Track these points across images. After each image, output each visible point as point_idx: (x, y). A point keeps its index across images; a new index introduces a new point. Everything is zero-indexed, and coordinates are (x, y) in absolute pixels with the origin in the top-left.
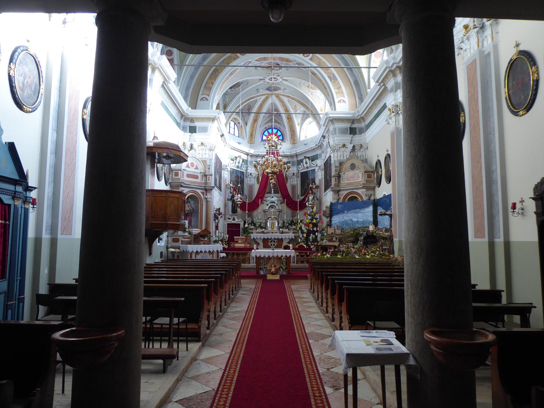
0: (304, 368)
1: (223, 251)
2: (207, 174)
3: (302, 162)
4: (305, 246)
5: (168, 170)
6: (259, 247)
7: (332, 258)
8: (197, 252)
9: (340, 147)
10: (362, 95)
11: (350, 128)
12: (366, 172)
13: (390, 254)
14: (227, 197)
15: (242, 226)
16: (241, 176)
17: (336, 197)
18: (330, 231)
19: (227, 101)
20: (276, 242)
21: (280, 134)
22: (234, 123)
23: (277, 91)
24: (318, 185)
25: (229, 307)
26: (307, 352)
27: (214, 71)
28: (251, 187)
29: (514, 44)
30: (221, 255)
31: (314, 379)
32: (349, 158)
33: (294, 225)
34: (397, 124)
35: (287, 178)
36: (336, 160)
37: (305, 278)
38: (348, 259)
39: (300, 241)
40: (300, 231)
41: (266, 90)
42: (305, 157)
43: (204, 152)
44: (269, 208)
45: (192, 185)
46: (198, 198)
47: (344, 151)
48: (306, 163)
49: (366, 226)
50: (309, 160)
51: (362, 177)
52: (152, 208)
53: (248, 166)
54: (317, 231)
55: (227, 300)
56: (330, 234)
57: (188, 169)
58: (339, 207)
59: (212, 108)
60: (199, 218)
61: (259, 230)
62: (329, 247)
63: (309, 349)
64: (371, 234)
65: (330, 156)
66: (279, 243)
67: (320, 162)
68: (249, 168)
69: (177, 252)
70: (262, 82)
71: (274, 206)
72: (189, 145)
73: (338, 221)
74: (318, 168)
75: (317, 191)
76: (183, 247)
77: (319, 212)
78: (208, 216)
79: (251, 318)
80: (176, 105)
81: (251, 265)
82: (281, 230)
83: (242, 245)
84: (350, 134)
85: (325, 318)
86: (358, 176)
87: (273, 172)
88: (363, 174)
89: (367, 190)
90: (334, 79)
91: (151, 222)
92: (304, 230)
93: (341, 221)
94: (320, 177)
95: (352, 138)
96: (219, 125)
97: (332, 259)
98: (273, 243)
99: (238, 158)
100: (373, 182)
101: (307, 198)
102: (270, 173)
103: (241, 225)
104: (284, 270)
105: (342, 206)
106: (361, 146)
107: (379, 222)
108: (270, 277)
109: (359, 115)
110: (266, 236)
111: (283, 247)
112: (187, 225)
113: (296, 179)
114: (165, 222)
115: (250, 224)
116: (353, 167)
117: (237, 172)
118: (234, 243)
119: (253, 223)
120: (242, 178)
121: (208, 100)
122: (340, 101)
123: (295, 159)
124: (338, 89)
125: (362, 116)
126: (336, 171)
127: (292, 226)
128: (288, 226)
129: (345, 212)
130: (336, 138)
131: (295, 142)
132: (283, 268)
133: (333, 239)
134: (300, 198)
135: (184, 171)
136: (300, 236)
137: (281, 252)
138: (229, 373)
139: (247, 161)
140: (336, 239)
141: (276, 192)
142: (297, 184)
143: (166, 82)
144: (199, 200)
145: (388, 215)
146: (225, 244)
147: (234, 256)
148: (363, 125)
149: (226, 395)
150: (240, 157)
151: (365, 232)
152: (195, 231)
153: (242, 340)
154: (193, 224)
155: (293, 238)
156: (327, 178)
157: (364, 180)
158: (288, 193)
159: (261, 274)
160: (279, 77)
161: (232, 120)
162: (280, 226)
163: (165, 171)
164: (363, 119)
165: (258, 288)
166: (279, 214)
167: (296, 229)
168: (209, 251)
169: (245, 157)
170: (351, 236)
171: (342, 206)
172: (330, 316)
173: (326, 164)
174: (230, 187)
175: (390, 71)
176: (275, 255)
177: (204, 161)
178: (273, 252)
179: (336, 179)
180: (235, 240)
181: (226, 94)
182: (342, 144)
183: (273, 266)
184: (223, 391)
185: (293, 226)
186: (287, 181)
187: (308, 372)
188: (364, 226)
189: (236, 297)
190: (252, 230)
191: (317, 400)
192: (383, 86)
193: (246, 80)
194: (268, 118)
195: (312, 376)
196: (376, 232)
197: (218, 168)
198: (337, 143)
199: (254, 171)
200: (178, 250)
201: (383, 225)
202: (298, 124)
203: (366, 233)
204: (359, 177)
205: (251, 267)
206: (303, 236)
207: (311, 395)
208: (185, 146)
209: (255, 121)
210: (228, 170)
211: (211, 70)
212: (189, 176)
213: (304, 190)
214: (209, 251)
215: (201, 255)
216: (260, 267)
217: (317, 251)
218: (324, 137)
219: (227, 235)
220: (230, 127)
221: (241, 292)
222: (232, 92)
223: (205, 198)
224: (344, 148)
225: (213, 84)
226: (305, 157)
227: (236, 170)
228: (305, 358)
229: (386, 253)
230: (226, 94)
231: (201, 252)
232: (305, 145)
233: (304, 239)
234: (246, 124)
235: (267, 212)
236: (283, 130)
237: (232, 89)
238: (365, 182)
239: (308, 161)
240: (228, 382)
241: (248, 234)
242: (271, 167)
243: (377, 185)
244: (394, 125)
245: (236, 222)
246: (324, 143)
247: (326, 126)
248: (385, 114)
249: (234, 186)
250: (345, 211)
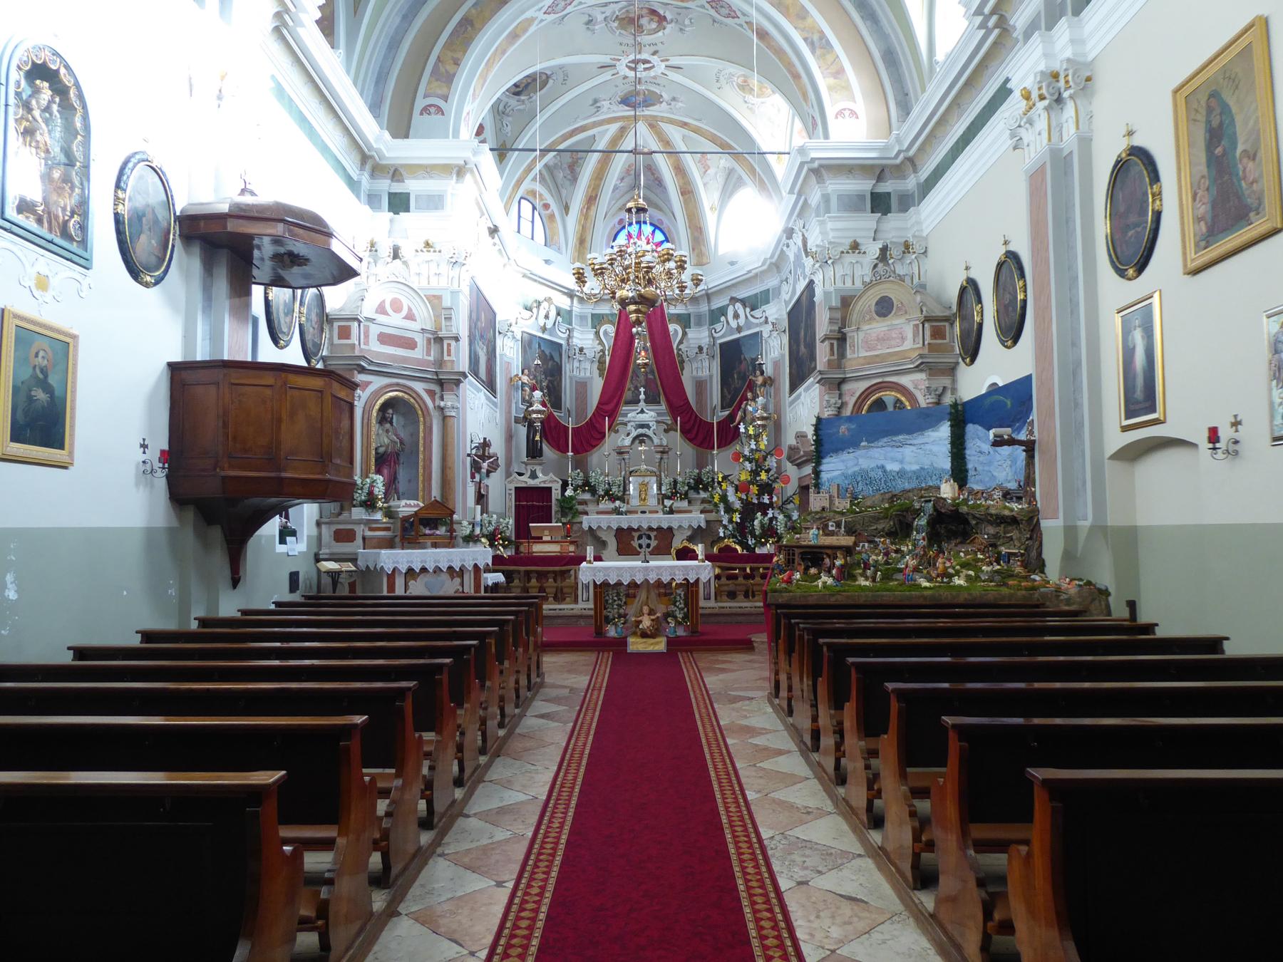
2: (442, 334)
3: (725, 314)
5: (314, 317)
6: (605, 554)
7: (842, 589)
8: (410, 571)
9: (842, 252)
11: (872, 193)
12: (928, 319)
13: (1029, 572)
14: (514, 414)
15: (556, 494)
16: (553, 354)
17: (834, 400)
19: (509, 135)
20: (653, 538)
22: (531, 206)
23: (651, 108)
25: (481, 785)
26: (740, 823)
27: (460, 24)
28: (582, 387)
29: (1124, 131)
30: (487, 578)
32: (872, 281)
33: (705, 489)
35: (682, 362)
36: (832, 289)
37: (746, 646)
38: (894, 591)
40: (722, 506)
44: (633, 442)
45: (395, 368)
46: (414, 408)
47: (854, 261)
48: (736, 316)
49: (930, 487)
50: (745, 306)
51: (915, 335)
52: (225, 425)
53: (573, 329)
54: (771, 505)
56: (817, 513)
57: (381, 318)
58: (843, 429)
59: (456, 134)
61: (606, 505)
62: (829, 551)
63: (747, 817)
65: (810, 285)
66: (662, 541)
67: (777, 311)
68: (576, 334)
70: (607, 76)
72: (389, 250)
73: (839, 472)
74: (770, 327)
75: (767, 393)
76: (367, 556)
77: (775, 449)
78: (449, 464)
79: (581, 758)
80: (339, 117)
81: (581, 605)
82: (668, 503)
83: (553, 549)
84: (872, 212)
85: (836, 805)
86: (901, 333)
87: (641, 296)
88: (917, 326)
89: (930, 375)
90: (821, 48)
91: (223, 473)
92: (733, 502)
93: (850, 472)
95: (878, 222)
97: (844, 591)
98: (644, 541)
99: (545, 305)
102: (633, 301)
103: (553, 491)
104: (680, 623)
105: (853, 427)
106: (907, 247)
107: (971, 473)
108: (636, 645)
110: (624, 522)
111: (673, 551)
112: (379, 490)
113: (706, 364)
114: (273, 474)
115: (581, 487)
116: (885, 307)
117: (542, 344)
118: (529, 543)
119: (587, 486)
122: (840, 113)
123: (704, 308)
124: (835, 78)
125: (911, 153)
126: (832, 321)
127: (699, 493)
128: (686, 494)
129: (863, 444)
130: (830, 225)
131: (705, 261)
132: (675, 617)
134: (720, 414)
139: (570, 312)
140: (838, 525)
142: (711, 377)
145: (1020, 443)
146: (501, 545)
147: (529, 581)
148: (911, 183)
149: (544, 873)
150: (549, 300)
151: (931, 504)
152: (407, 505)
154: (402, 485)
155: (703, 525)
156: (798, 352)
157: (921, 345)
158: (687, 399)
159: (608, 635)
160: (655, 57)
161: (526, 197)
162: (663, 492)
163: (303, 319)
164: (912, 163)
165: (598, 685)
166: (661, 458)
167: (710, 502)
168: (450, 568)
169: (564, 302)
170: (885, 515)
171: (853, 427)
172: (829, 763)
173: (794, 314)
174: (523, 383)
176: (652, 578)
177: (434, 296)
178: (646, 569)
179: (832, 345)
181: (503, 113)
182: (848, 242)
183: (646, 609)
185: (701, 491)
186: (683, 369)
187: (749, 888)
188: (923, 485)
189: (518, 731)
190: (586, 504)
191: (751, 880)
192: (996, 26)
193: (561, 67)
194: (626, 193)
196: (969, 501)
197: (482, 324)
198: (832, 240)
199: (591, 342)
200: (349, 567)
201: (987, 479)
204: (903, 339)
205: (579, 613)
206: (731, 521)
208: (376, 251)
209: (591, 200)
210: (514, 338)
212: (384, 339)
213: (729, 393)
214: (450, 568)
215: (422, 579)
218: (789, 233)
220: (519, 217)
221: (539, 706)
222: (521, 107)
223: (439, 407)
224: (854, 252)
225: (457, 63)
227: (540, 337)
231: (424, 570)
232: (732, 263)
234: (566, 208)
235: (628, 452)
236: (671, 227)
237: (522, 98)
238: (926, 351)
239: (741, 311)
240: (524, 924)
241: (573, 517)
242: (634, 281)
243: (963, 359)
244: (1045, 141)
246: (788, 253)
247: (800, 194)
248: (1006, 115)
250: (862, 441)
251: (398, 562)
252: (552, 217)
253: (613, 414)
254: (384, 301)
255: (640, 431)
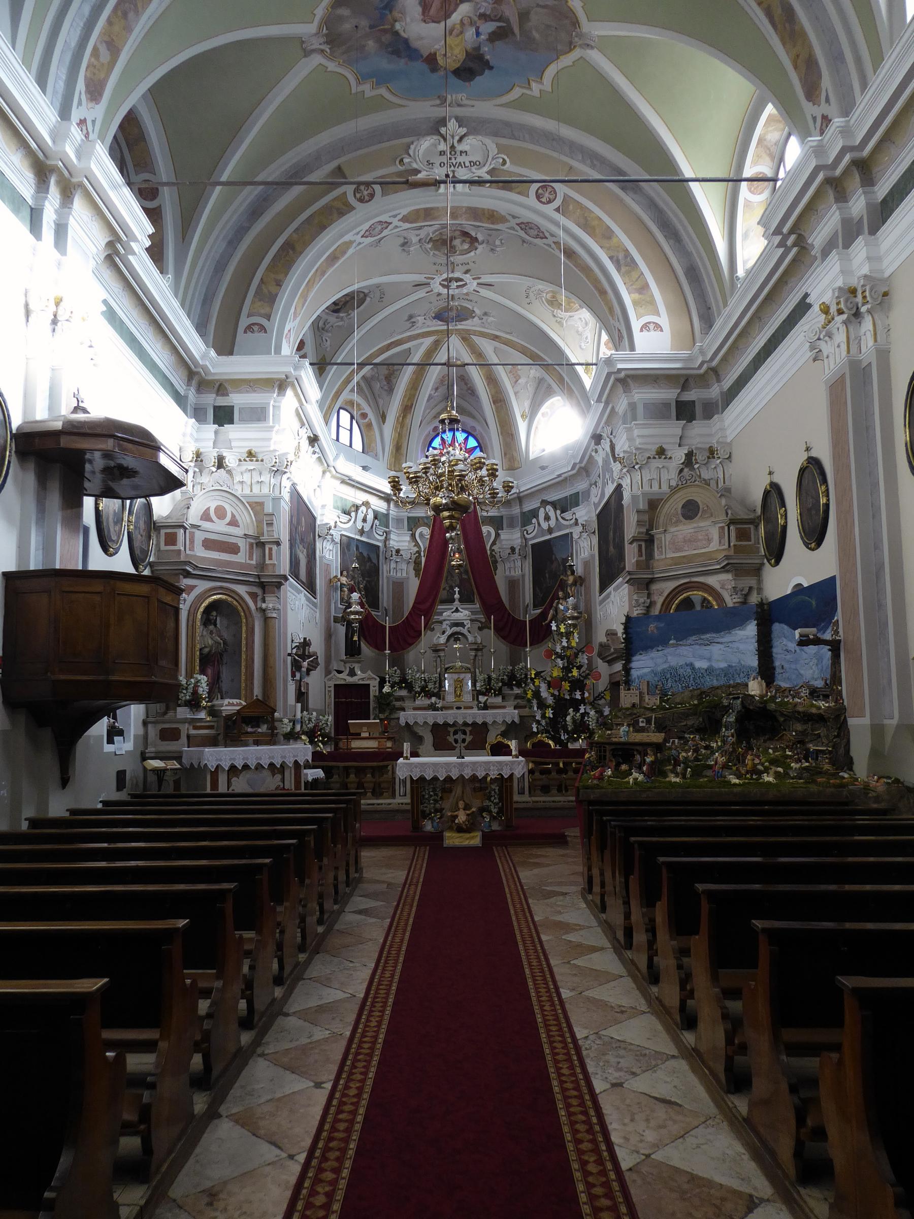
0: (536, 1011)
1: (317, 763)
2: (263, 539)
4: (551, 742)
5: (142, 525)
8: (233, 768)
9: (649, 458)
10: (710, 308)
11: (676, 401)
12: (732, 522)
13: (837, 769)
14: (333, 614)
15: (374, 691)
18: (627, 699)
21: (476, 444)
24: (580, 574)
27: (282, 248)
28: (399, 587)
30: (307, 774)
31: (559, 1036)
32: (678, 485)
33: (519, 685)
34: (854, 350)
35: (495, 562)
36: (640, 493)
37: (560, 840)
39: (535, 730)
41: (434, 318)
42: (544, 503)
43: (256, 478)
46: (240, 616)
47: (661, 466)
48: (547, 518)
49: (738, 684)
50: (555, 509)
51: (721, 537)
54: (583, 701)
55: (342, 887)
56: (627, 709)
57: (206, 525)
58: (652, 627)
60: (243, 667)
61: (422, 701)
64: (761, 706)
67: (586, 513)
68: (392, 536)
69: (171, 769)
70: (421, 293)
71: (462, 634)
73: (649, 670)
74: (580, 528)
81: (398, 800)
82: (482, 699)
83: (372, 744)
84: (677, 420)
86: (707, 535)
87: (454, 502)
89: (736, 575)
93: (659, 669)
94: (586, 554)
95: (683, 429)
96: (301, 405)
97: (655, 788)
98: (460, 736)
99: (363, 509)
100: (754, 550)
101: (551, 612)
102: (446, 507)
103: (372, 688)
105: (662, 625)
107: (778, 670)
108: (452, 839)
109: (706, 362)
110: (440, 717)
111: (488, 746)
112: (203, 689)
114: (101, 678)
116: (691, 510)
118: (347, 739)
119: (404, 682)
120: (375, 561)
121: (265, 330)
123: (516, 510)
124: (640, 293)
125: (714, 363)
127: (512, 689)
128: (500, 689)
129: (671, 642)
130: (636, 432)
131: (516, 465)
133: (638, 722)
135: (194, 530)
136: (535, 717)
137: (485, 763)
138: (366, 1026)
139: (387, 515)
140: (648, 721)
141: (466, 599)
142: (523, 576)
143: (119, 246)
144: (242, 614)
145: (826, 642)
148: (714, 392)
149: (361, 1073)
150: (366, 504)
151: (739, 701)
152: (230, 704)
153: (382, 996)
154: (225, 685)
155: (517, 720)
157: (726, 546)
159: (424, 830)
160: (468, 275)
162: (478, 689)
163: (132, 527)
164: (715, 373)
166: (476, 656)
168: (272, 765)
169: (379, 505)
170: (694, 711)
171: (662, 625)
173: (602, 516)
175: (828, 183)
176: (467, 774)
177: (256, 503)
179: (640, 546)
180: (352, 731)
182: (655, 448)
183: (461, 804)
184: (354, 1066)
185: (515, 688)
186: (496, 569)
187: (564, 1090)
188: (732, 682)
189: (336, 927)
190: (403, 700)
191: (566, 1082)
192: (794, 245)
193: (378, 286)
195: (554, 1028)
199: (407, 544)
201: (794, 677)
202: (522, 416)
203: (742, 702)
204: (709, 540)
205: (396, 807)
206: (543, 716)
207: (560, 1108)
208: (202, 461)
209: (407, 408)
210: (333, 541)
211: (276, 244)
212: (209, 544)
214: (272, 765)
216: (421, 807)
217: (601, 761)
218: (597, 438)
219: (327, 717)
221: (359, 902)
222: (341, 323)
223: (261, 608)
224: (660, 458)
225: (279, 284)
226: (544, 503)
228: (536, 989)
229: (827, 767)
230: (323, 329)
231: (246, 767)
233: (546, 723)
234: (383, 417)
235: (444, 650)
237: (341, 315)
238: (732, 552)
239: (552, 513)
240: (366, 1046)
241: (390, 714)
242: (447, 488)
243: (769, 561)
244: (844, 353)
245: (359, 680)
247: (607, 403)
248: (806, 328)
249: (352, 582)
251: (221, 760)
252: (369, 425)
253: (428, 612)
254: (208, 509)
255: (455, 629)
